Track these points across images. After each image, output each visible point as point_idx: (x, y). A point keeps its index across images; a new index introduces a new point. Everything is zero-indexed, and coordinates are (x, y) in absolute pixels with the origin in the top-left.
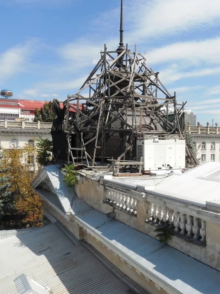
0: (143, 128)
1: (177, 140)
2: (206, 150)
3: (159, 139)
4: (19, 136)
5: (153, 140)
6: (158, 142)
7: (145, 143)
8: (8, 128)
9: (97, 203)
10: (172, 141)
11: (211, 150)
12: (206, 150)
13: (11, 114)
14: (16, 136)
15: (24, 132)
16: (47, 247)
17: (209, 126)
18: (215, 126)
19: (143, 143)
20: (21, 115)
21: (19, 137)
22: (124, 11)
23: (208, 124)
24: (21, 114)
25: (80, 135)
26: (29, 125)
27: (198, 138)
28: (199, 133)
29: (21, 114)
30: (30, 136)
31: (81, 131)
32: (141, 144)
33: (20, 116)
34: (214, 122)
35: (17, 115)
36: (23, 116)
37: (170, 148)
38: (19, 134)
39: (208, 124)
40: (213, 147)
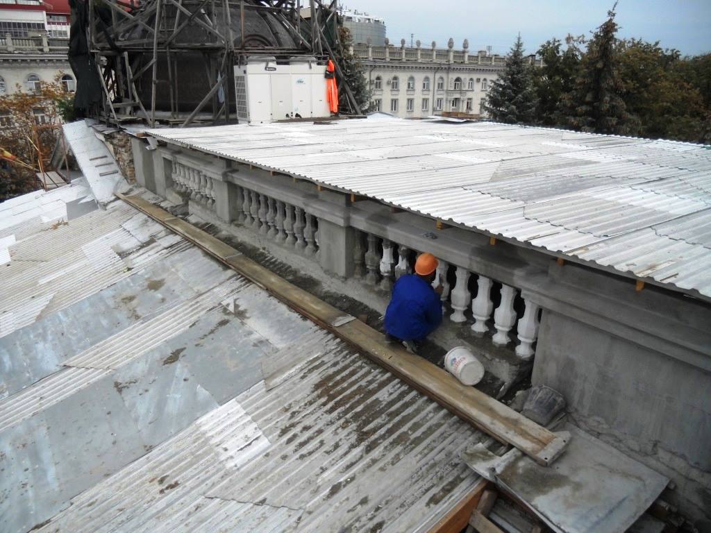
0: (250, 42)
1: (314, 65)
2: (382, 90)
3: (278, 63)
4: (41, 67)
5: (264, 65)
6: (275, 69)
7: (248, 72)
8: (16, 52)
9: (707, 67)
10: (304, 67)
11: (408, 91)
12: (398, 90)
13: (33, 24)
14: (35, 69)
15: (49, 60)
16: (108, 207)
17: (406, 45)
18: (415, 46)
19: (245, 72)
20: (49, 26)
21: (42, 70)
22: (509, 284)
23: (403, 42)
24: (49, 23)
25: (123, 59)
26: (27, 43)
27: (386, 69)
28: (388, 60)
29: (49, 23)
30: (29, 68)
31: (125, 50)
32: (242, 74)
33: (47, 27)
34: (415, 40)
35: (40, 26)
36: (54, 27)
37: (300, 82)
38: (40, 65)
39: (403, 42)
40: (411, 85)
